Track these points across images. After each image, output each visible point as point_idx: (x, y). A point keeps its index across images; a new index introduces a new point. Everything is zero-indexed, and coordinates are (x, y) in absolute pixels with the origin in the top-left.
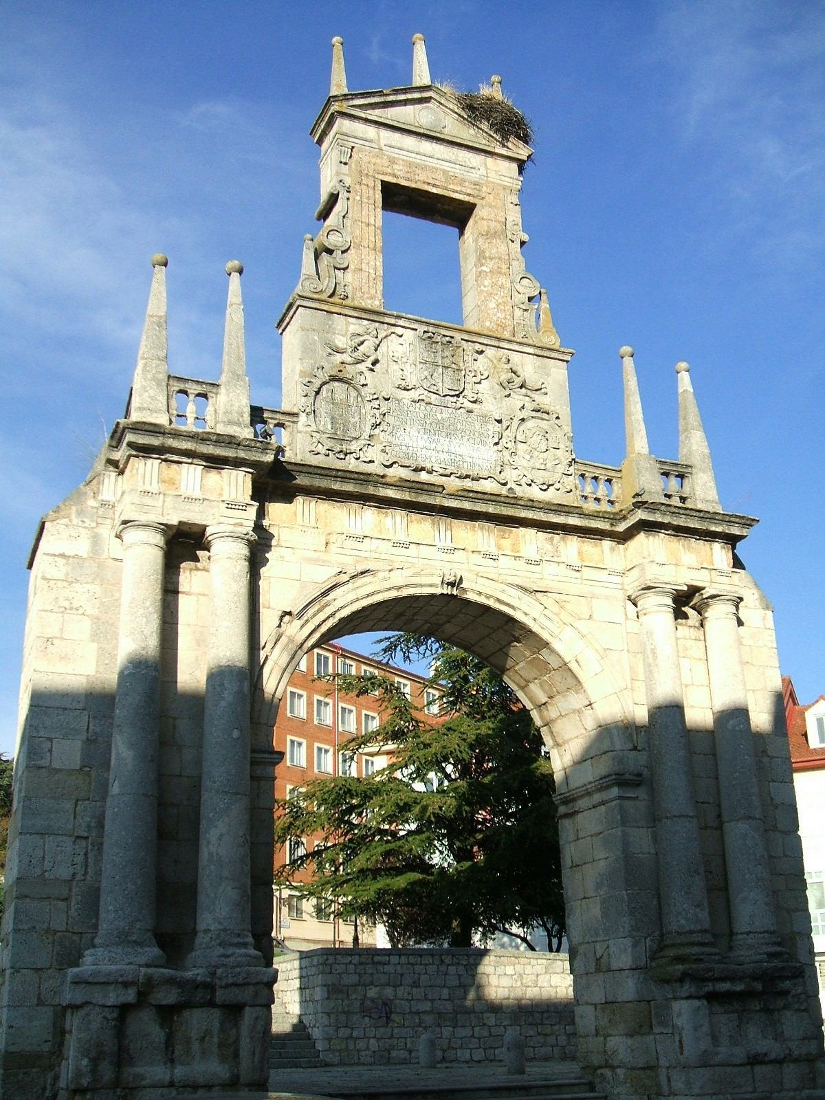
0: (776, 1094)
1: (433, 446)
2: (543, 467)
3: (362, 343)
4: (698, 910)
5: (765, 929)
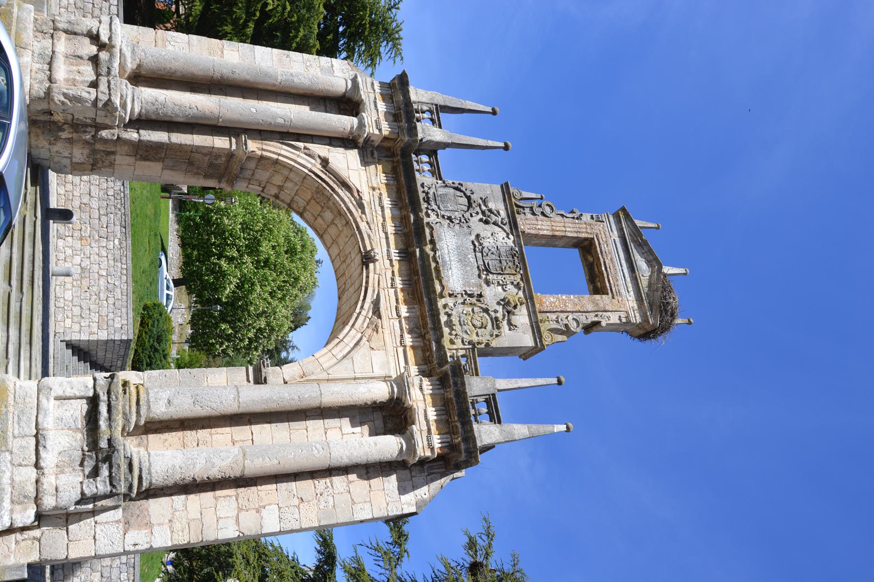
0: (9, 458)
1: (452, 252)
2: (462, 323)
3: (496, 216)
4: (166, 401)
5: (153, 465)
